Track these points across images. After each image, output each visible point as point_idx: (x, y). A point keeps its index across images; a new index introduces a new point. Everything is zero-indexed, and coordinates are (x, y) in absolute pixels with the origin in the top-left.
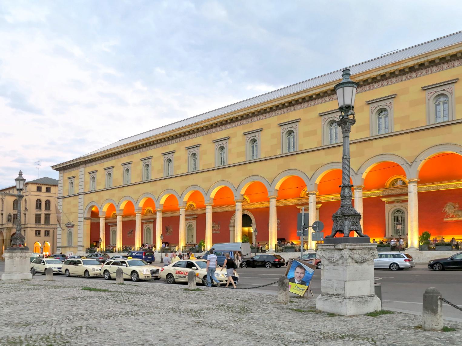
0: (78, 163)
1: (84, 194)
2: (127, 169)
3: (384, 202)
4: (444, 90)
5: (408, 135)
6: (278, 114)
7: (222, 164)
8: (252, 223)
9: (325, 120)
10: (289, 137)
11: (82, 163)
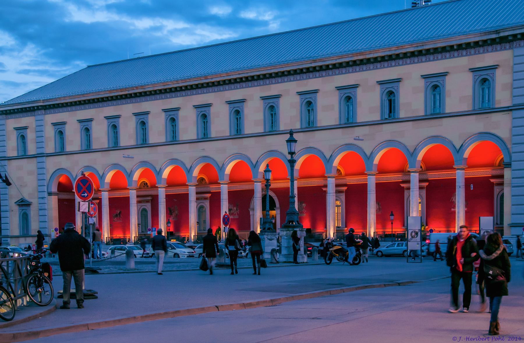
0: (34, 107)
1: (47, 156)
2: (114, 125)
3: (403, 187)
4: (487, 75)
5: (411, 123)
6: (471, 54)
7: (309, 125)
8: (275, 207)
9: (428, 84)
10: (434, 93)
11: (40, 108)
